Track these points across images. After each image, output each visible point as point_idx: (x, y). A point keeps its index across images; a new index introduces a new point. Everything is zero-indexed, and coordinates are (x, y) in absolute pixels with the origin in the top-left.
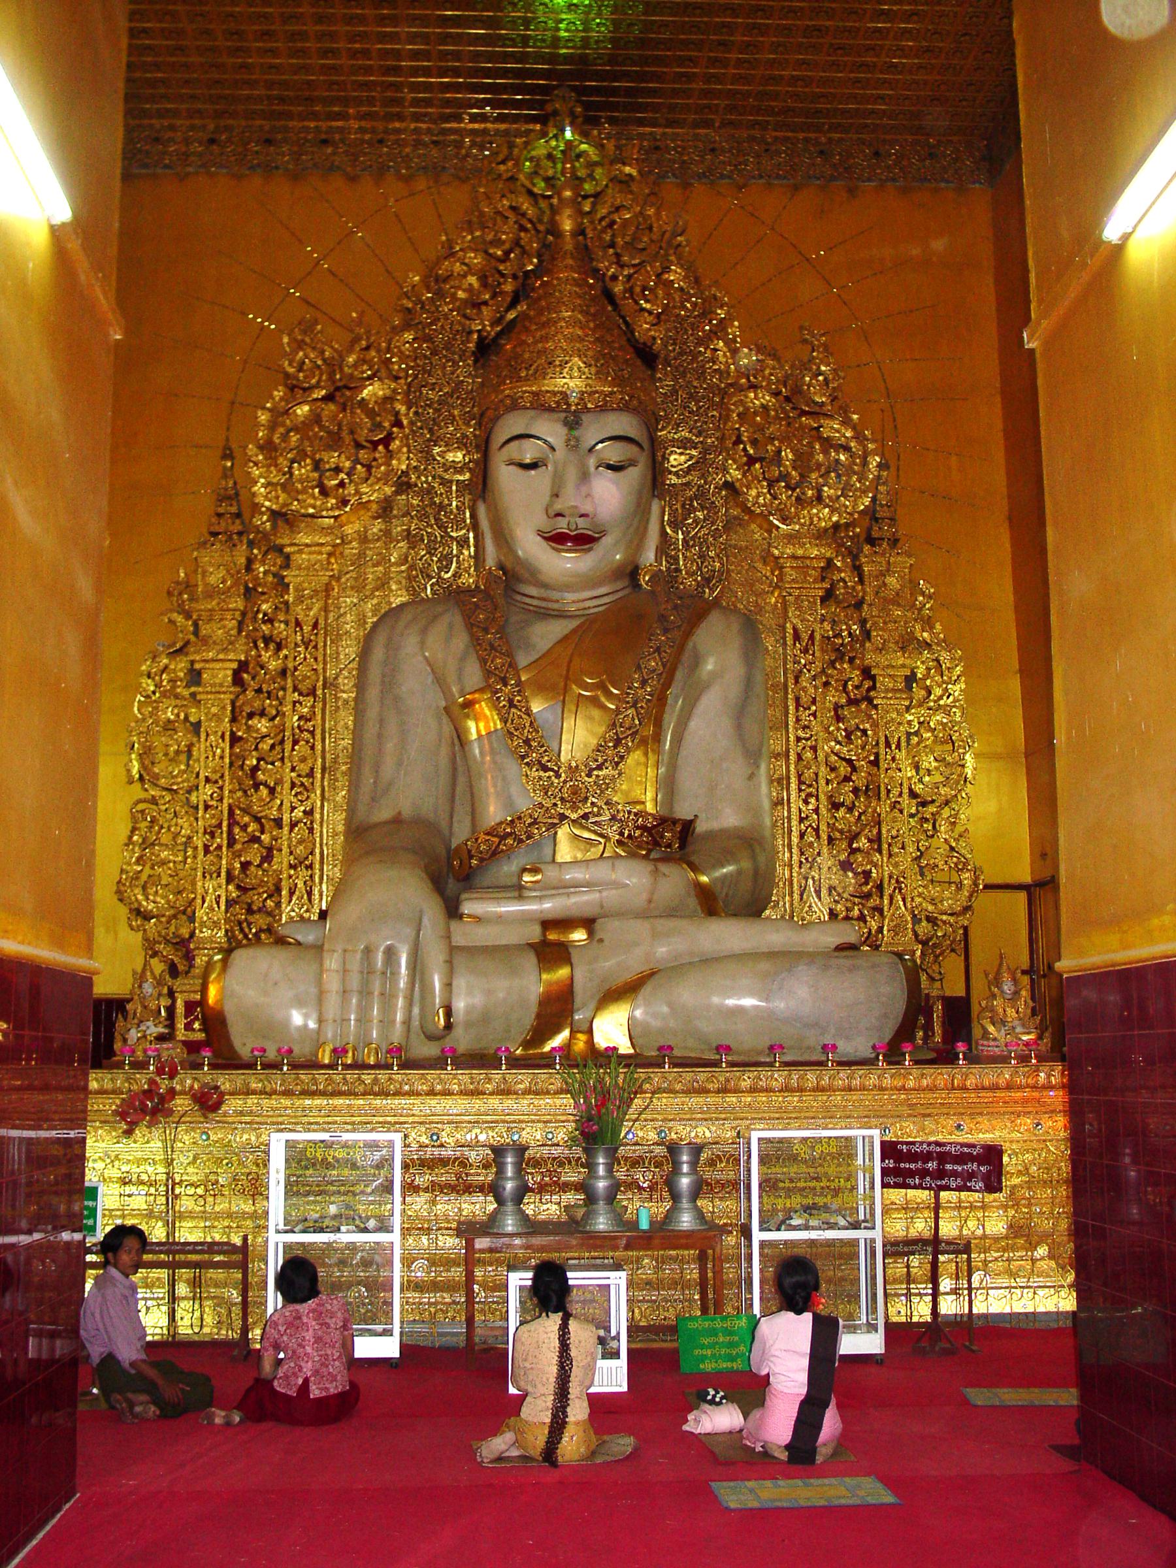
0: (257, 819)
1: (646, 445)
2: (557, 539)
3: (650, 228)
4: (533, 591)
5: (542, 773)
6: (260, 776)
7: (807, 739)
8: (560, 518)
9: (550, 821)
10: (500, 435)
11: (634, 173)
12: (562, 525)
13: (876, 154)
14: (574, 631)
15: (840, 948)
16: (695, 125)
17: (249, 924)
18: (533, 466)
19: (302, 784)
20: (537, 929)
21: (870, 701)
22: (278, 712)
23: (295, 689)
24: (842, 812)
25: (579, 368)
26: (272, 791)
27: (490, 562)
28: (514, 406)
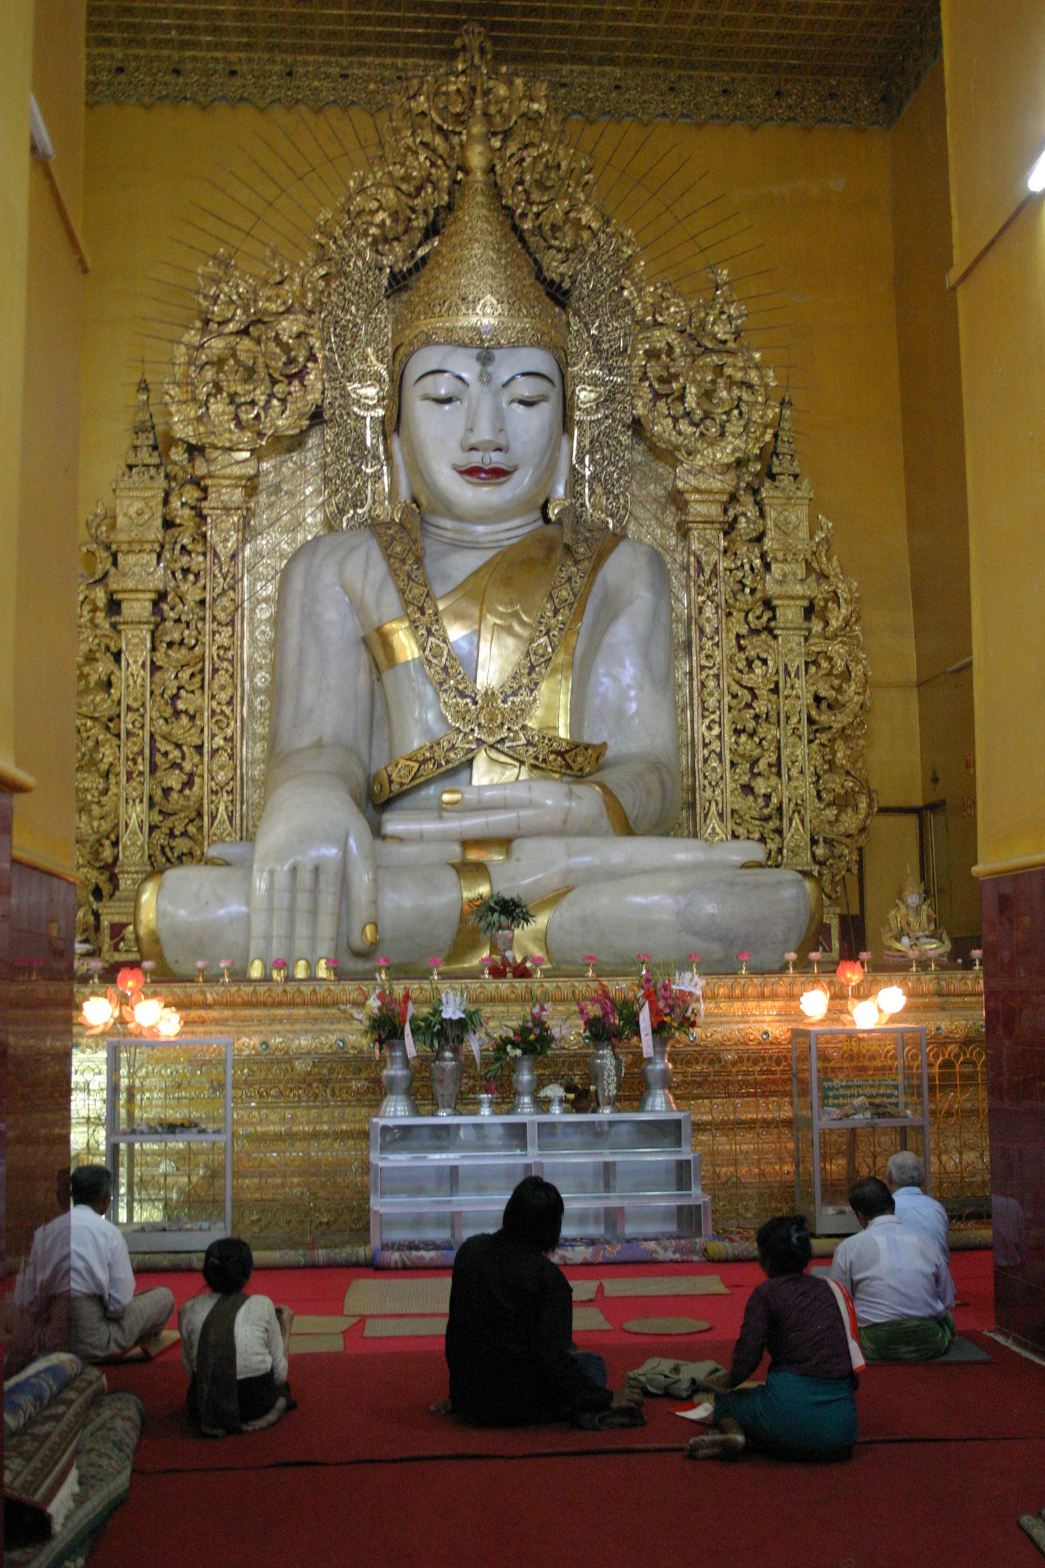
0: (178, 746)
1: (557, 379)
2: (472, 472)
3: (559, 166)
4: (448, 523)
5: (459, 700)
6: (181, 705)
7: (710, 668)
8: (473, 453)
9: (467, 746)
10: (415, 369)
11: (543, 109)
12: (475, 459)
13: (778, 94)
14: (487, 564)
15: (745, 866)
16: (601, 62)
17: (172, 849)
18: (448, 400)
19: (222, 712)
20: (457, 848)
21: (770, 630)
22: (197, 641)
23: (214, 618)
24: (743, 738)
25: (492, 305)
26: (192, 718)
27: (404, 495)
28: (428, 341)
